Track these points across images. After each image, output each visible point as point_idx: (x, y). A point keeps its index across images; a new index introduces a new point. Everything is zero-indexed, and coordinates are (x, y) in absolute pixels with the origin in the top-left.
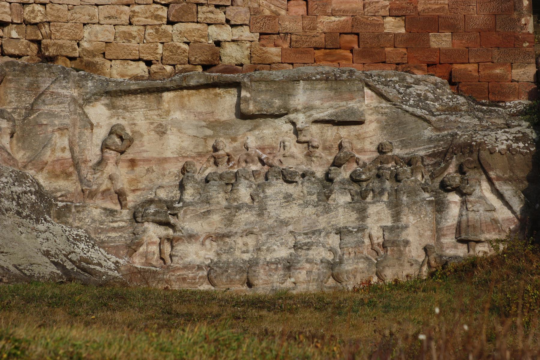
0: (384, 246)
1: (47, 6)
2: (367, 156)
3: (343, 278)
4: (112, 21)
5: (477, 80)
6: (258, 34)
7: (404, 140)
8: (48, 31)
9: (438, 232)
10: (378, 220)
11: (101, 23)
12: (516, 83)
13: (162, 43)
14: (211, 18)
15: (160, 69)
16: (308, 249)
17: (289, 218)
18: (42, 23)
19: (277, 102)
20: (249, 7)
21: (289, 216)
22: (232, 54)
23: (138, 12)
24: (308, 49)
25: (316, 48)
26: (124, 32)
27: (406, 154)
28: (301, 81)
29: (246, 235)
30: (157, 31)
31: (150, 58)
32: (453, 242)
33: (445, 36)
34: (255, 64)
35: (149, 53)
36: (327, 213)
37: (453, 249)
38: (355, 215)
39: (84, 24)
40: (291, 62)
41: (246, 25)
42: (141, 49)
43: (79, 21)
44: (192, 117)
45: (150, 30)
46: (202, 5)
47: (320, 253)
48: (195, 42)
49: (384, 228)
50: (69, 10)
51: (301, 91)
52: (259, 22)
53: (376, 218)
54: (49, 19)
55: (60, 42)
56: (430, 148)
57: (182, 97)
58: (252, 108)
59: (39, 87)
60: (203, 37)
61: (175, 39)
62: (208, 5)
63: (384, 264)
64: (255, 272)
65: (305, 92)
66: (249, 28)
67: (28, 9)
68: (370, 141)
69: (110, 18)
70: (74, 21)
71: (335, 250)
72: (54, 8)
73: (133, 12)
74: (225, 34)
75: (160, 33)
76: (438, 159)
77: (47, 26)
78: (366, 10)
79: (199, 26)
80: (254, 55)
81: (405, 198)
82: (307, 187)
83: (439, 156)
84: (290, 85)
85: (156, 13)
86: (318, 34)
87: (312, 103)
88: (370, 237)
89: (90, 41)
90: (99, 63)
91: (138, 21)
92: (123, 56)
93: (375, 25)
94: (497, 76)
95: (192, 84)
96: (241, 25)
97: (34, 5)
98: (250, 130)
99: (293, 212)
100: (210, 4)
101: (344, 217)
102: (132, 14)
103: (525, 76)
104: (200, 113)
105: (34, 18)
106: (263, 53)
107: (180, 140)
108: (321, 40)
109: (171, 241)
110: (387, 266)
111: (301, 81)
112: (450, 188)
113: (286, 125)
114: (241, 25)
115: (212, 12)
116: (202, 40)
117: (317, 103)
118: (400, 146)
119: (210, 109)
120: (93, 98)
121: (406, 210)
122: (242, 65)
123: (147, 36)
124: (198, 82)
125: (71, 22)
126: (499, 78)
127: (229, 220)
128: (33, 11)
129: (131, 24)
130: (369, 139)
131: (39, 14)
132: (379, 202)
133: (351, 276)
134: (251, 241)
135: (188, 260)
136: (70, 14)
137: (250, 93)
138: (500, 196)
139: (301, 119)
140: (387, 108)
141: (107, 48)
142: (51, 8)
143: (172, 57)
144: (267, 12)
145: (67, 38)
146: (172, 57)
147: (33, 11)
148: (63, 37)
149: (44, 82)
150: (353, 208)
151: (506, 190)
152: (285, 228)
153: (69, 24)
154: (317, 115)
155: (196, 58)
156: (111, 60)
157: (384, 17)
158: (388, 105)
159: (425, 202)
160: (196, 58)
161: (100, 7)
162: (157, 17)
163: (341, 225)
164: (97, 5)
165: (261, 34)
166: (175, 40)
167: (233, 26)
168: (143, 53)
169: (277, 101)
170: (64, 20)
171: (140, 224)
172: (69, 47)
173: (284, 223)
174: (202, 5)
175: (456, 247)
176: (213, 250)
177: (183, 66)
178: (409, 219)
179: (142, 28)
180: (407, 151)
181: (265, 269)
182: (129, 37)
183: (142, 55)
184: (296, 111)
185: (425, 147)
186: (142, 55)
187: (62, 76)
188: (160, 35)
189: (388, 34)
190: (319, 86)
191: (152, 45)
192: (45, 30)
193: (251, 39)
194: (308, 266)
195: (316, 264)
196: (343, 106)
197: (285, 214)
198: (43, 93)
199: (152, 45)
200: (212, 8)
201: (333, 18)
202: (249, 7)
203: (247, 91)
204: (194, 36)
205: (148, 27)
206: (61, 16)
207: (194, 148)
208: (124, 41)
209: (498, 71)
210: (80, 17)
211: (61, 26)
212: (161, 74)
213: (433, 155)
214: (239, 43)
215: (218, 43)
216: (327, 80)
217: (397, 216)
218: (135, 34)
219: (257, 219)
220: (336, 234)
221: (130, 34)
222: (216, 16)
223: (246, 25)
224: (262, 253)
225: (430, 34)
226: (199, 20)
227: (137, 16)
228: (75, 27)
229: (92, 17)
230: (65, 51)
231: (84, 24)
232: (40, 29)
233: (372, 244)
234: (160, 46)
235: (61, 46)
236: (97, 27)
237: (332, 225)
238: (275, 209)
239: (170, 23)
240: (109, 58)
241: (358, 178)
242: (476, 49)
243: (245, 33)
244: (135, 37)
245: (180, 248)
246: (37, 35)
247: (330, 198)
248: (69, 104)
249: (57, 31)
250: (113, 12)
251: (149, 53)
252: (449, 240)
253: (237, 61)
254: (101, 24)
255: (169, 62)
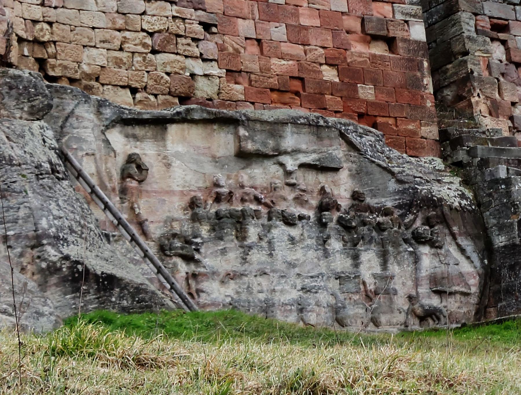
0: (376, 293)
1: (54, 25)
2: (345, 203)
3: (347, 322)
4: (106, 45)
5: (397, 134)
6: (225, 71)
7: (373, 190)
8: (54, 51)
9: (417, 283)
10: (370, 268)
11: (97, 46)
12: (425, 140)
13: (148, 72)
14: (189, 50)
15: (145, 98)
16: (316, 292)
17: (295, 260)
18: (49, 42)
19: (271, 143)
20: (216, 43)
21: (294, 258)
22: (204, 89)
23: (129, 39)
24: (265, 90)
25: (272, 90)
26: (116, 58)
27: (376, 203)
28: (289, 124)
29: (261, 275)
30: (144, 59)
31: (137, 85)
32: (427, 292)
33: (370, 88)
34: (223, 100)
35: (136, 81)
36: (327, 258)
37: (427, 299)
38: (349, 262)
39: (84, 46)
40: (252, 101)
41: (215, 60)
42: (130, 76)
43: (81, 42)
44: (192, 150)
45: (138, 58)
46: (180, 36)
47: (324, 297)
48: (176, 73)
49: (375, 276)
50: (71, 31)
51: (289, 134)
52: (225, 59)
53: (368, 265)
54: (56, 39)
55: (65, 63)
56: (396, 200)
57: (183, 130)
58: (250, 146)
59: (64, 110)
60: (182, 69)
61: (159, 69)
62: (186, 37)
63: (379, 311)
64: (273, 312)
65: (292, 135)
66: (216, 63)
67: (38, 26)
68: (345, 188)
69: (104, 42)
70: (76, 43)
71: (336, 294)
72: (59, 27)
73: (125, 37)
74: (198, 67)
75: (147, 61)
76: (404, 211)
77: (53, 46)
78: (308, 56)
79: (178, 57)
80: (223, 92)
81: (390, 249)
82: (307, 230)
83: (404, 208)
84: (280, 127)
85: (144, 41)
86: (272, 76)
87: (299, 147)
88: (364, 283)
89: (89, 64)
90: (95, 87)
91: (128, 48)
92: (115, 82)
93: (314, 71)
94: (410, 130)
95: (195, 118)
96: (211, 60)
97: (43, 23)
98: (243, 169)
99: (298, 255)
100: (188, 37)
101: (341, 263)
102: (124, 40)
103: (431, 134)
104: (199, 147)
105: (43, 37)
106: (230, 90)
107: (184, 173)
108: (274, 81)
109: (195, 276)
110: (381, 313)
111: (289, 124)
112: (424, 240)
113: (274, 166)
114: (211, 60)
115: (189, 45)
116: (181, 72)
117: (304, 147)
118: (370, 195)
119: (207, 145)
120: (111, 125)
121: (391, 260)
122: (210, 100)
123: (135, 63)
124: (201, 116)
125: (73, 43)
126: (414, 133)
127: (243, 259)
128: (42, 30)
129: (121, 49)
130: (343, 186)
131: (47, 33)
132: (369, 250)
133: (353, 320)
134: (264, 281)
135: (214, 296)
136: (72, 35)
137: (248, 132)
138: (463, 251)
139: (290, 163)
140: (355, 156)
141: (102, 72)
142: (57, 28)
143: (156, 86)
144: (231, 50)
145: (71, 59)
146: (156, 86)
147: (42, 30)
148: (67, 58)
149: (69, 104)
150: (348, 254)
151: (468, 246)
152: (293, 270)
153: (72, 45)
154: (304, 159)
155: (176, 89)
156: (103, 85)
157: (321, 64)
158: (356, 154)
159: (407, 253)
160: (176, 89)
161: (97, 30)
162: (145, 45)
163: (339, 270)
164: (93, 28)
165: (228, 71)
166: (159, 70)
167: (204, 60)
168: (132, 80)
169: (270, 142)
170: (68, 41)
171: (168, 258)
172: (72, 69)
173: (292, 265)
174: (180, 36)
175: (429, 297)
176: (231, 288)
177: (164, 96)
178: (394, 268)
179: (130, 54)
180: (376, 201)
181: (281, 310)
182: (119, 63)
183: (131, 82)
184: (286, 153)
185: (391, 198)
186: (131, 82)
187: (84, 99)
188: (147, 63)
189: (326, 81)
190: (304, 130)
191: (140, 73)
192: (51, 49)
193: (220, 75)
194: (317, 309)
195: (324, 307)
196: (325, 152)
197: (291, 257)
198: (69, 116)
199: (140, 73)
200: (189, 41)
201: (283, 62)
202: (216, 43)
203: (245, 130)
204: (175, 67)
205: (137, 54)
206: (66, 36)
207: (196, 182)
208: (115, 66)
209: (410, 127)
210: (81, 40)
211: (65, 47)
212: (146, 103)
213: (399, 207)
214: (210, 78)
215: (193, 75)
216: (310, 125)
217: (384, 265)
218: (125, 60)
219: (267, 260)
220: (336, 279)
221: (121, 60)
222: (193, 49)
223: (215, 60)
224: (276, 293)
225: (359, 85)
226: (179, 51)
227: (128, 43)
228: (77, 49)
229: (91, 40)
230: (69, 73)
231: (84, 46)
232: (45, 47)
233: (366, 291)
234: (146, 74)
235: (65, 67)
236: (94, 51)
237: (331, 270)
238: (283, 252)
239: (154, 52)
240: (102, 82)
241: (348, 225)
242: (393, 104)
243: (214, 70)
244: (125, 63)
245: (205, 285)
246: (43, 54)
247: (327, 243)
248: (93, 129)
249: (63, 51)
250: (107, 36)
251: (136, 81)
252: (424, 289)
253: (208, 95)
254: (98, 48)
255: (153, 91)
